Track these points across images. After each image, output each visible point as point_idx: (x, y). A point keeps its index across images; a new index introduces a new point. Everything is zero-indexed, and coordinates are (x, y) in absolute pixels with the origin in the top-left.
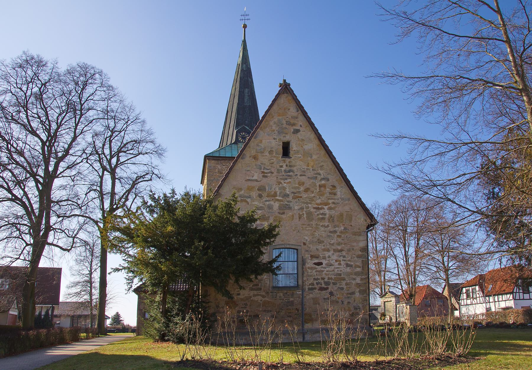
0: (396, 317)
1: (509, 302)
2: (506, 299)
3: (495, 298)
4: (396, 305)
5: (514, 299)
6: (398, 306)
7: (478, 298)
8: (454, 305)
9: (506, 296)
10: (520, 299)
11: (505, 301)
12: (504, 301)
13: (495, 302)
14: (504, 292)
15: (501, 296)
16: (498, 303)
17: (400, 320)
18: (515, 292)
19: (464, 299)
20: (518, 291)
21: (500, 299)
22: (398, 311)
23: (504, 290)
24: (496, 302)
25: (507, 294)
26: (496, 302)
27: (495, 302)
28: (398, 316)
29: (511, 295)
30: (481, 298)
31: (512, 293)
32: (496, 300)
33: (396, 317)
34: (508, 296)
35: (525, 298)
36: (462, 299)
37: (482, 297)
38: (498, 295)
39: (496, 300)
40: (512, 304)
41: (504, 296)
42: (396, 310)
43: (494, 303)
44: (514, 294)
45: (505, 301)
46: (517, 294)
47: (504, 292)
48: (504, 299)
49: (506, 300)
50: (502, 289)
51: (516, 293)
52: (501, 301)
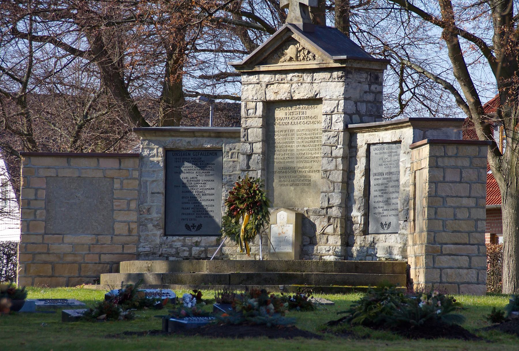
17: (373, 244)
22: (359, 181)
28: (357, 215)
35: (475, 199)
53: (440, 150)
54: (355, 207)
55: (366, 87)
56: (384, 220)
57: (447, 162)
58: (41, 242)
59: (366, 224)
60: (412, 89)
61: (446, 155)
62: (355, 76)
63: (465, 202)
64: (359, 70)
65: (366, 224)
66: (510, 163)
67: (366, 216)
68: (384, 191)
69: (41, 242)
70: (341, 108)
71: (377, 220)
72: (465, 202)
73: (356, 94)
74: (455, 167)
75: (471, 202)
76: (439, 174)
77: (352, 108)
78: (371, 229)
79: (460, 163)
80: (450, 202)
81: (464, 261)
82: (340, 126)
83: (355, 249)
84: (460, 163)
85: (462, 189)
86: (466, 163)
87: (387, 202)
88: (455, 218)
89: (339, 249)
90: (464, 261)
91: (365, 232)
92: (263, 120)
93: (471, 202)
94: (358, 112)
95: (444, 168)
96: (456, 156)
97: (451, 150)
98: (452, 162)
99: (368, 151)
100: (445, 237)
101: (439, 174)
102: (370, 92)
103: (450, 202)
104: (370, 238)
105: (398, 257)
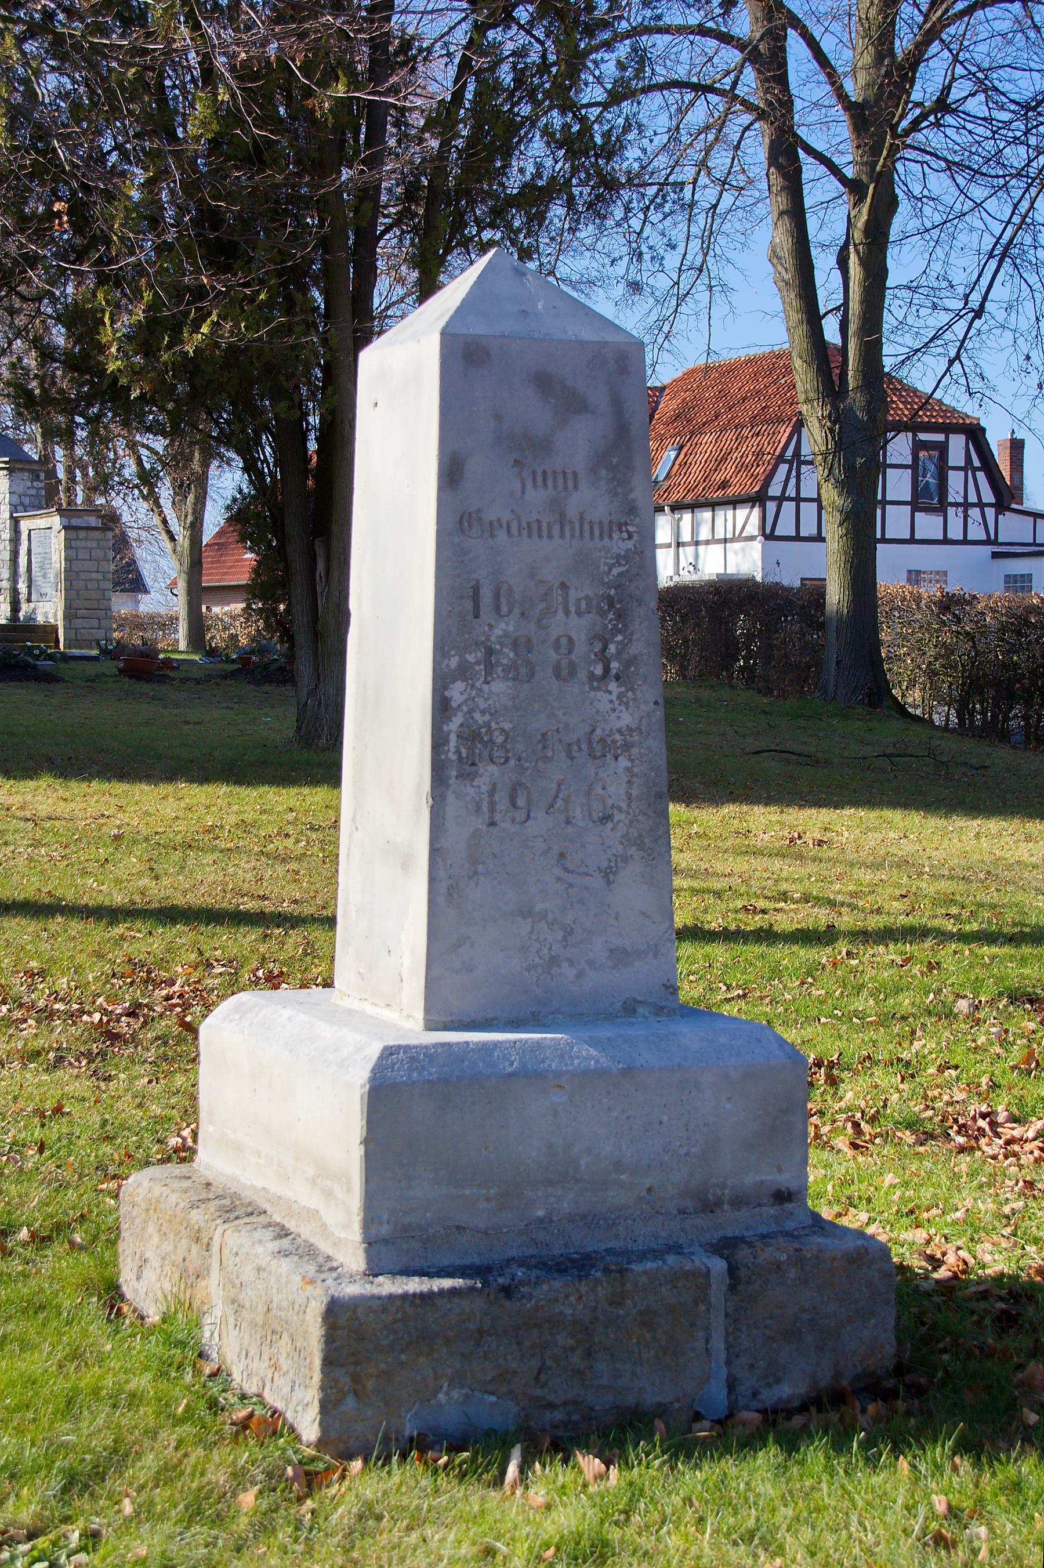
0: (15, 592)
1: (743, 550)
2: (729, 536)
3: (680, 519)
4: (15, 522)
5: (769, 536)
6: (25, 525)
7: (951, 511)
8: (954, 398)
9: (730, 513)
10: (798, 538)
11: (725, 541)
12: (719, 541)
13: (679, 545)
14: (720, 493)
15: (707, 515)
16: (690, 550)
17: (34, 611)
18: (773, 498)
19: (798, 500)
20: (791, 492)
21: (704, 534)
22: (23, 560)
23: (724, 485)
24: (684, 544)
25: (735, 503)
26: (684, 544)
27: (679, 545)
28: (22, 587)
29: (756, 512)
30: (974, 513)
31: (759, 499)
32: (686, 537)
33: (15, 592)
34: (742, 513)
35: (917, 537)
36: (781, 499)
37: (981, 505)
38: (694, 507)
39: (686, 537)
40: (754, 562)
41: (720, 514)
42: (15, 554)
43: (672, 550)
44: (771, 506)
45: (725, 541)
46: (789, 507)
47: (720, 493)
48: (720, 534)
49: (733, 540)
50: (718, 477)
51: (781, 499)
52: (707, 542)
53: (73, 534)
54: (21, 581)
55: (29, 484)
56: (43, 591)
57: (78, 544)
58: (908, 537)
59: (30, 594)
60: (752, 538)
61: (77, 539)
62: (19, 475)
63: (94, 575)
64: (22, 470)
65: (30, 594)
66: (182, 546)
67: (29, 587)
68: (42, 568)
69: (908, 537)
70: (7, 500)
71: (38, 591)
72: (94, 575)
73: (20, 489)
74: (85, 548)
75: (100, 576)
76: (73, 553)
77: (16, 500)
78: (33, 598)
79: (89, 544)
80: (83, 576)
81: (94, 623)
82: (7, 515)
83: (21, 615)
84: (89, 544)
85: (90, 565)
86: (95, 545)
87: (44, 576)
88: (87, 589)
89: (9, 614)
90: (94, 623)
91: (29, 600)
92: (653, 538)
93: (100, 576)
94: (22, 504)
95: (77, 549)
96: (86, 539)
97: (82, 534)
98: (83, 544)
99: (29, 535)
100: (77, 603)
101: (73, 553)
102: (33, 487)
103: (83, 576)
104: (32, 605)
105: (52, 621)
